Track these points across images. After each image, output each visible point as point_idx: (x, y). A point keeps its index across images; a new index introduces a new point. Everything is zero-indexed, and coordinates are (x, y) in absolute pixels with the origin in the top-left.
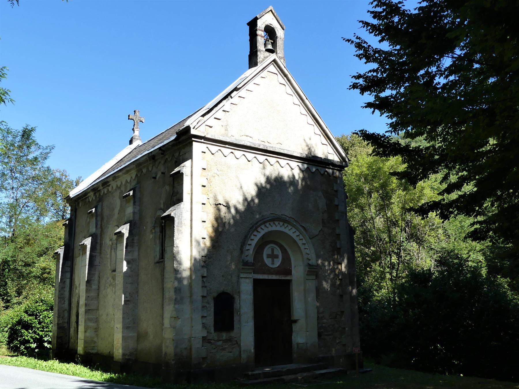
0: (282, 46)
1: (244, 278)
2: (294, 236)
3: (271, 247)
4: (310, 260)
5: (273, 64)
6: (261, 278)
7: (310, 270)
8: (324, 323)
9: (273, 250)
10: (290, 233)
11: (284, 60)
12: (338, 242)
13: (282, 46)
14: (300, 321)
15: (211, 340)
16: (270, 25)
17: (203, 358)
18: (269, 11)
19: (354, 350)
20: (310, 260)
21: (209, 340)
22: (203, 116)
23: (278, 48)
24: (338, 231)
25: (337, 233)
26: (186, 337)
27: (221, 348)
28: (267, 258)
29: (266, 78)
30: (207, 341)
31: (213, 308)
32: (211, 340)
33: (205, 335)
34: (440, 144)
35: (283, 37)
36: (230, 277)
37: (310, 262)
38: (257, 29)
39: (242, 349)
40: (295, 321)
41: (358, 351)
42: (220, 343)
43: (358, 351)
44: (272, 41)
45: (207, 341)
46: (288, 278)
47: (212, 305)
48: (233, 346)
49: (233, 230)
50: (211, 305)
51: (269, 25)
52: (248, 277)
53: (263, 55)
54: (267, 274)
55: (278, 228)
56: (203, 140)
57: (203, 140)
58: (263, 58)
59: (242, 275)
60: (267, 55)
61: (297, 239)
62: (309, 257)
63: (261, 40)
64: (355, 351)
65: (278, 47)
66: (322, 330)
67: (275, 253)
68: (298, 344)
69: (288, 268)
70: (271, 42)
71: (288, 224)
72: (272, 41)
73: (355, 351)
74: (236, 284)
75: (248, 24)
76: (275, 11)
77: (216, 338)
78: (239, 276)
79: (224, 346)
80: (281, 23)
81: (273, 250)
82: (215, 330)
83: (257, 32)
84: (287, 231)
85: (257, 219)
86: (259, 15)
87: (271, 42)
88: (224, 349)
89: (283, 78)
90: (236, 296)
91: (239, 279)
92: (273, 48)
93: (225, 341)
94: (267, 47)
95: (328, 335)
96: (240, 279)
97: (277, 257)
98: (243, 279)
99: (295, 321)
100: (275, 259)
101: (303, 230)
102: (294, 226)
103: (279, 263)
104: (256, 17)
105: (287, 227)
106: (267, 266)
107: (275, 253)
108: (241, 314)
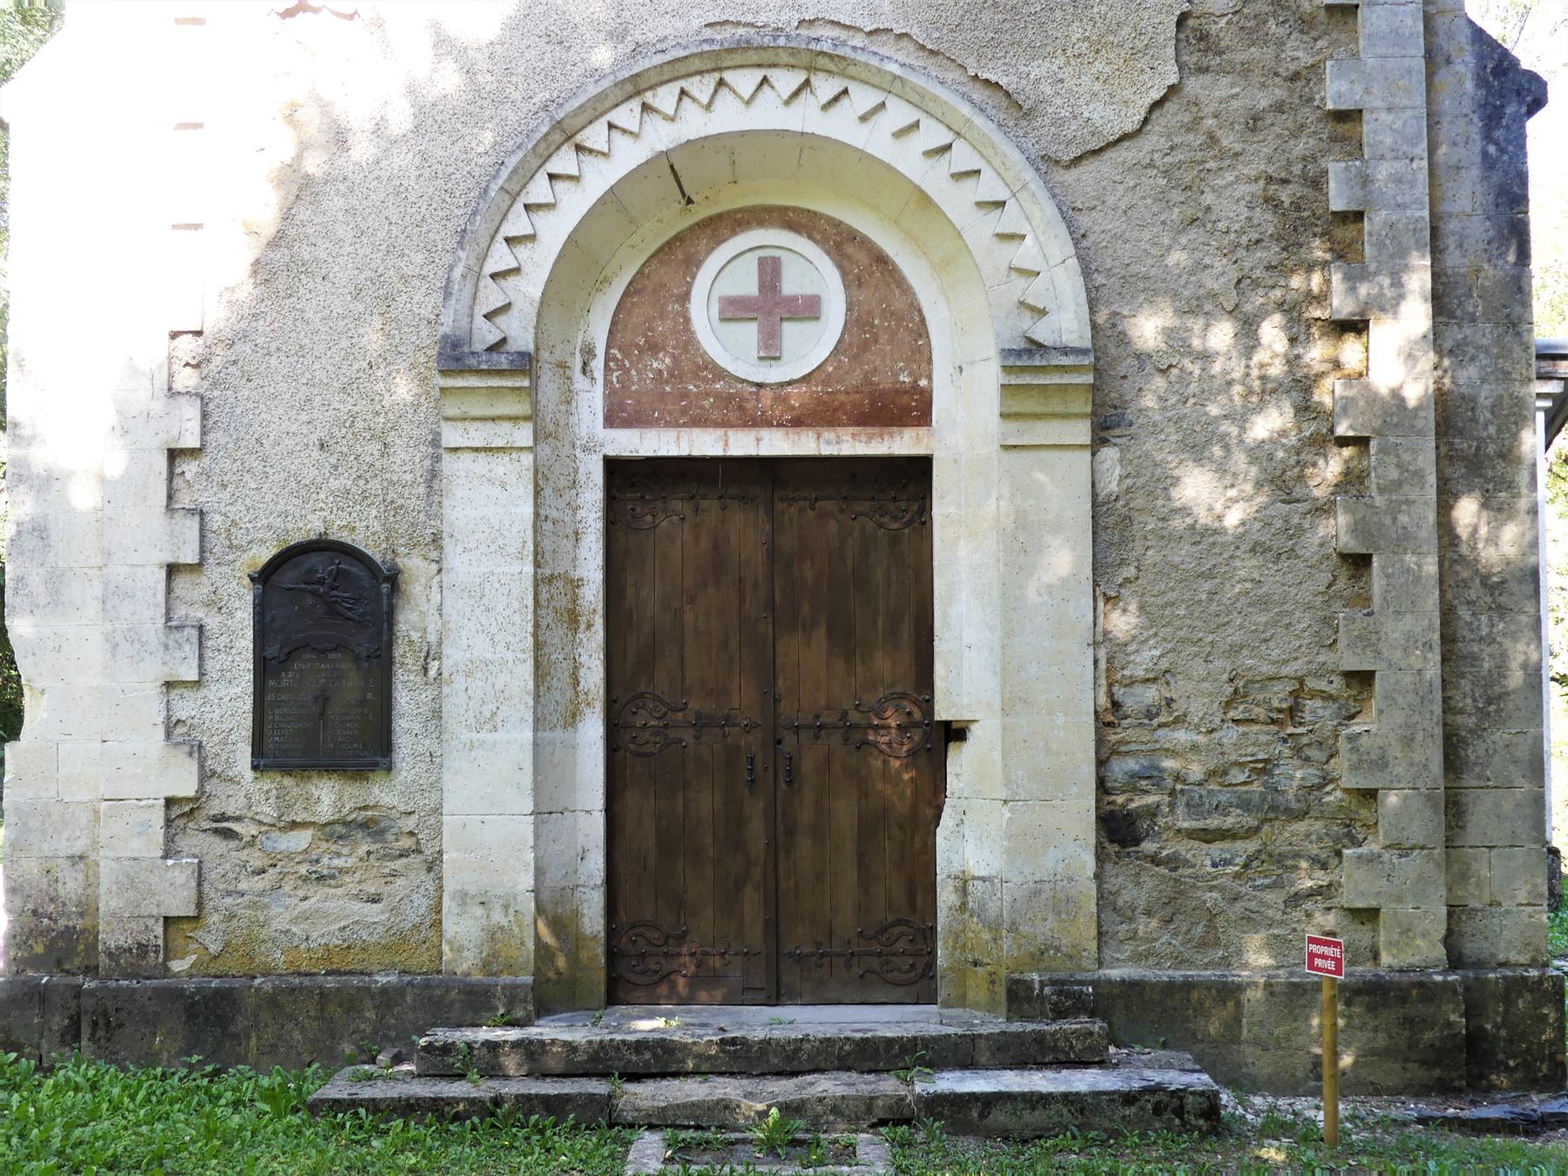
1: (476, 450)
2: (908, 159)
3: (760, 253)
4: (1043, 313)
6: (663, 452)
7: (1014, 380)
8: (1172, 753)
9: (770, 271)
10: (876, 140)
12: (1335, 169)
14: (973, 727)
15: (238, 819)
17: (168, 921)
19: (1312, 956)
20: (1043, 313)
21: (223, 817)
24: (1336, 91)
25: (1330, 106)
26: (79, 798)
27: (303, 870)
28: (723, 320)
30: (206, 825)
31: (250, 633)
32: (238, 819)
33: (188, 789)
36: (375, 448)
37: (1043, 332)
39: (450, 885)
40: (955, 733)
41: (1330, 965)
42: (300, 840)
43: (1330, 965)
45: (206, 825)
46: (901, 443)
47: (244, 617)
48: (399, 864)
49: (403, 160)
50: (239, 614)
52: (500, 443)
54: (717, 425)
55: (769, 114)
59: (452, 436)
61: (933, 179)
62: (1035, 292)
64: (1318, 962)
66: (1151, 799)
67: (793, 284)
68: (963, 884)
69: (905, 378)
71: (844, 75)
73: (1318, 962)
74: (422, 490)
77: (268, 811)
78: (435, 442)
79: (325, 860)
81: (770, 271)
82: (263, 759)
84: (841, 126)
85: (595, 74)
88: (321, 878)
90: (414, 565)
91: (437, 459)
93: (340, 830)
95: (1207, 836)
96: (446, 456)
97: (808, 309)
98: (467, 457)
99: (955, 733)
100: (789, 328)
102: (894, 86)
103: (824, 352)
105: (765, 87)
106: (720, 373)
107: (793, 284)
108: (445, 675)
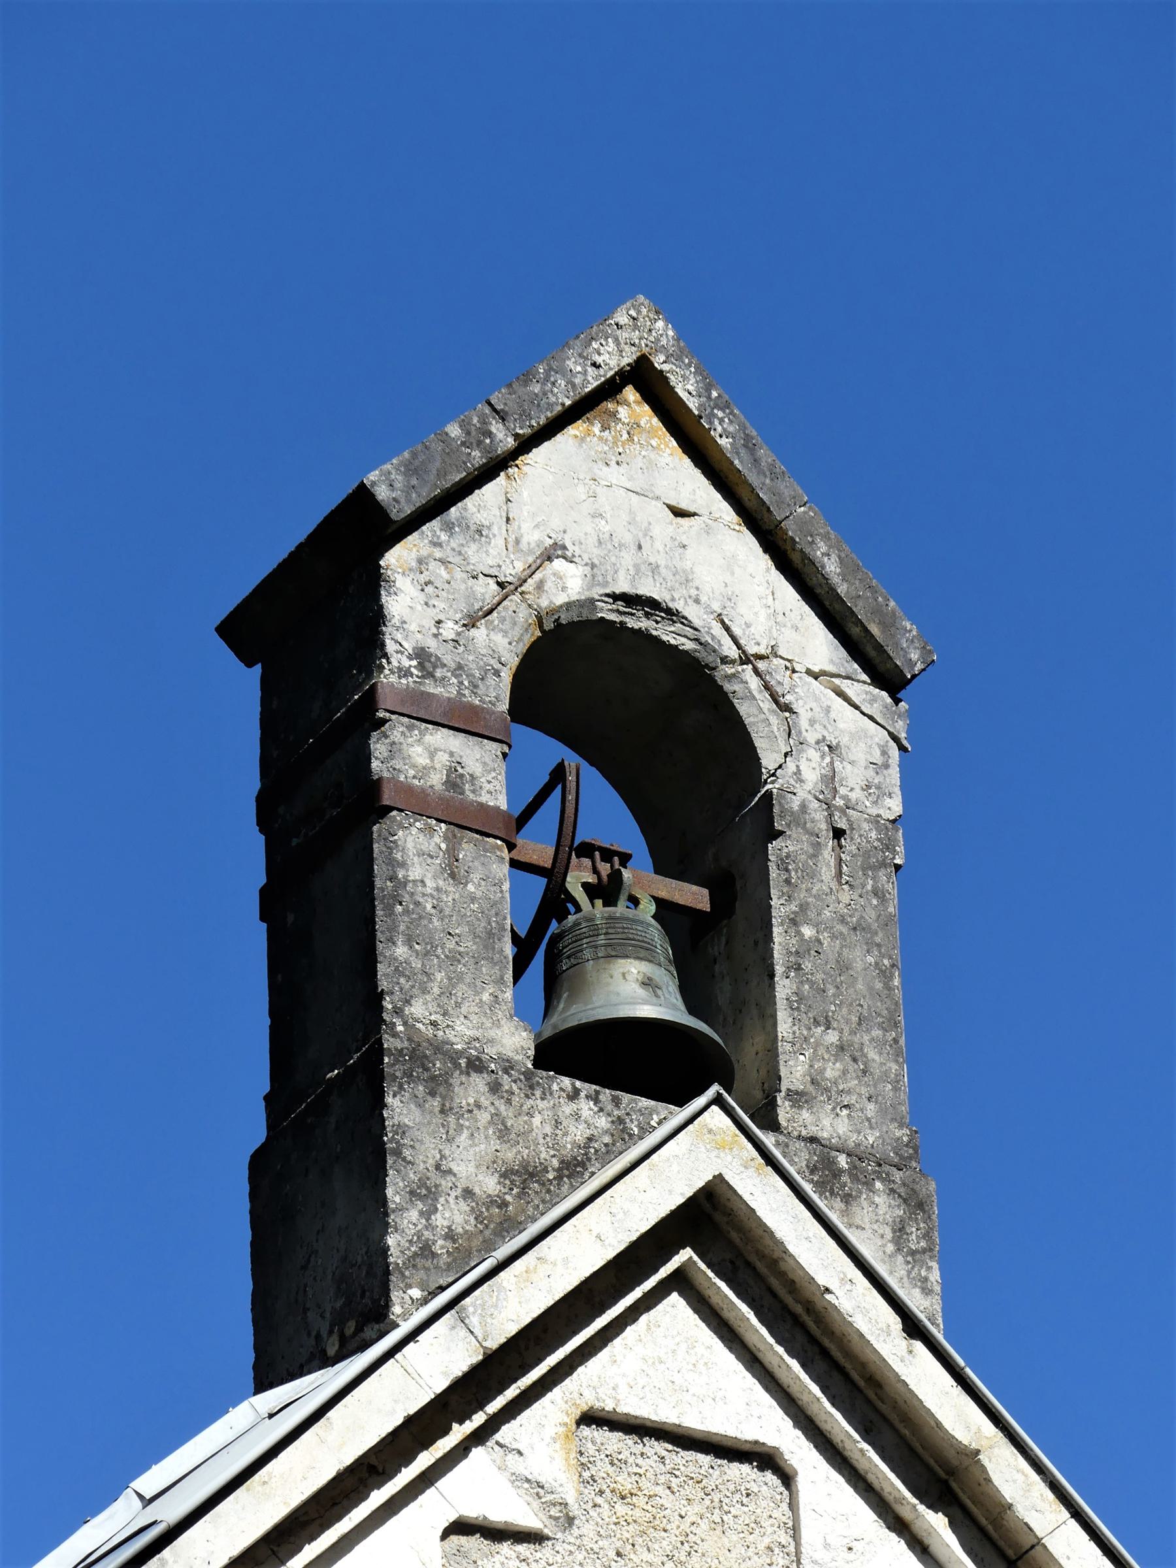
0: (862, 959)
5: (680, 1282)
11: (915, 1203)
13: (862, 959)
16: (638, 622)
18: (610, 390)
22: (154, 1523)
23: (798, 1003)
29: (564, 1541)
34: (492, 772)
35: (894, 806)
38: (371, 698)
44: (695, 896)
51: (607, 612)
53: (488, 1145)
56: (455, 1426)
57: (455, 1426)
58: (490, 1185)
60: (579, 1133)
63: (453, 871)
65: (784, 988)
70: (666, 910)
72: (695, 896)
75: (231, 630)
76: (708, 378)
80: (831, 567)
83: (378, 748)
86: (411, 470)
87: (666, 910)
89: (899, 1525)
92: (693, 1009)
94: (579, 988)
101: (968, 1371)
104: (362, 496)
